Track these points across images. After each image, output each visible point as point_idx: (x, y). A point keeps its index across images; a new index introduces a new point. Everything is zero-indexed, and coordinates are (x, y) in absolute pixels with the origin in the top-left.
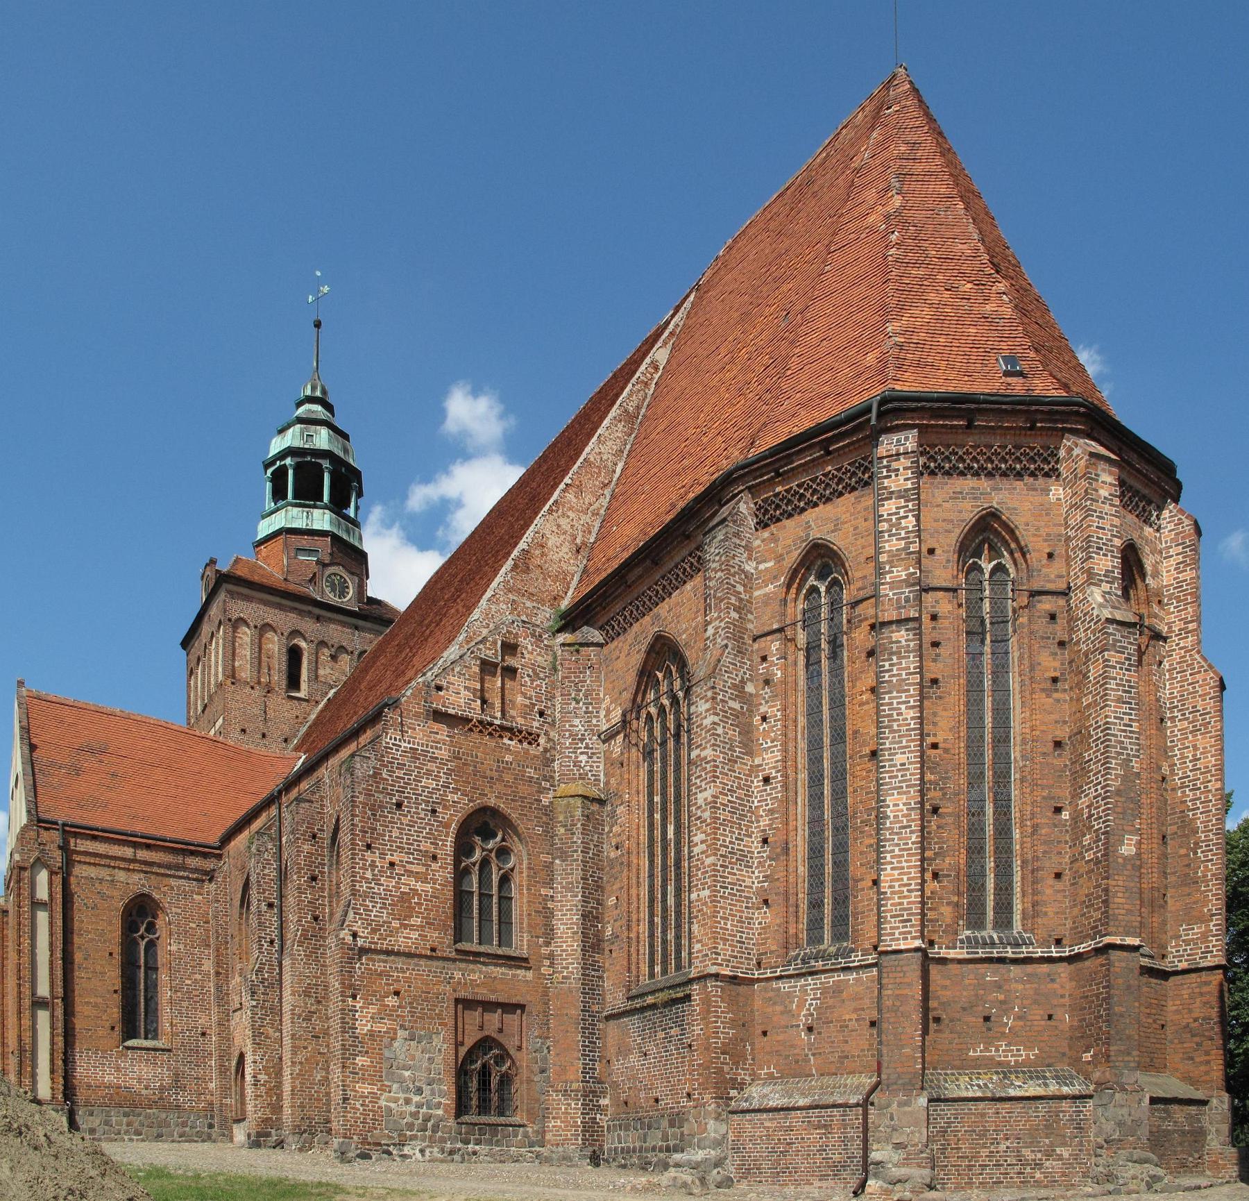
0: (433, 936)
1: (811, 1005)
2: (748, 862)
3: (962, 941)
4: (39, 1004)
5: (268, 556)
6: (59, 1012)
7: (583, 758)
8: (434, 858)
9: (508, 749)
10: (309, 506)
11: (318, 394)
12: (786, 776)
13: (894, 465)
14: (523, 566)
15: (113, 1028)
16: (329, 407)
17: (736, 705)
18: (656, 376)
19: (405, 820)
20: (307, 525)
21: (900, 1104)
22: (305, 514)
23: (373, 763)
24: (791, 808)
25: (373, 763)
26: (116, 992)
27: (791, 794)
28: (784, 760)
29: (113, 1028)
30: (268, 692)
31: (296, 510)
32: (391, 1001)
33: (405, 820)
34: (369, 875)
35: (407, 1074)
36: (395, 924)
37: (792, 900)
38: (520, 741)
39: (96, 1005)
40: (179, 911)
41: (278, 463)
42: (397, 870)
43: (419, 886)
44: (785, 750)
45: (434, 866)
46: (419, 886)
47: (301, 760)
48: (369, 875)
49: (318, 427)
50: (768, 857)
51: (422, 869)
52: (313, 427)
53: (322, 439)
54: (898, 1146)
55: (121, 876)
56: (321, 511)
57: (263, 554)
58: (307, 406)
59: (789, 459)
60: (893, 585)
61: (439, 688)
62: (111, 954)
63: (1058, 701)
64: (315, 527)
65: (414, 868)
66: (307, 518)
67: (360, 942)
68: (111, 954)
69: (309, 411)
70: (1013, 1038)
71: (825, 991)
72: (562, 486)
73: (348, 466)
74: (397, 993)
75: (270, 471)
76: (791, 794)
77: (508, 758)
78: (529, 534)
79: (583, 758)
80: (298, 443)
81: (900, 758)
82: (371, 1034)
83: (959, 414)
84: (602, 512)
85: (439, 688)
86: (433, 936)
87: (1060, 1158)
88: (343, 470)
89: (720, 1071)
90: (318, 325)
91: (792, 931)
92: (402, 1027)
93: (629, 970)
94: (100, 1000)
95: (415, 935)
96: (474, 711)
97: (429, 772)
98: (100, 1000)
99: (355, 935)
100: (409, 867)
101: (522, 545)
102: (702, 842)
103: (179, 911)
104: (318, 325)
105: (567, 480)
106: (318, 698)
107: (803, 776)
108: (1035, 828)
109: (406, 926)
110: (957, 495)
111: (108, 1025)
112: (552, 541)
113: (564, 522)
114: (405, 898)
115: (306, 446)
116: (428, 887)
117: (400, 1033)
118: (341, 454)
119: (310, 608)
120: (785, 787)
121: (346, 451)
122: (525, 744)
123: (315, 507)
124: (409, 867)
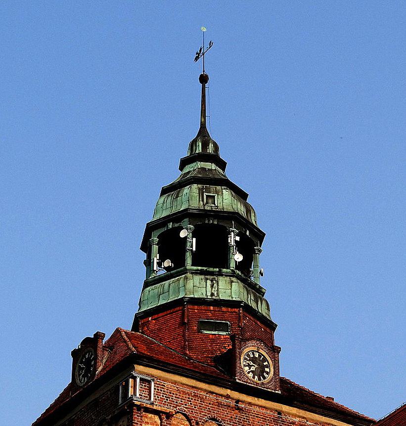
2: (158, 397)
5: (160, 330)
10: (212, 274)
11: (210, 149)
16: (222, 165)
20: (212, 294)
22: (209, 282)
31: (197, 278)
41: (170, 226)
49: (219, 188)
52: (213, 188)
56: (228, 279)
57: (151, 326)
64: (222, 297)
66: (212, 286)
69: (203, 169)
80: (196, 204)
88: (248, 233)
90: (204, 79)
104: (204, 79)
115: (207, 208)
119: (229, 392)
121: (249, 209)
123: (220, 274)
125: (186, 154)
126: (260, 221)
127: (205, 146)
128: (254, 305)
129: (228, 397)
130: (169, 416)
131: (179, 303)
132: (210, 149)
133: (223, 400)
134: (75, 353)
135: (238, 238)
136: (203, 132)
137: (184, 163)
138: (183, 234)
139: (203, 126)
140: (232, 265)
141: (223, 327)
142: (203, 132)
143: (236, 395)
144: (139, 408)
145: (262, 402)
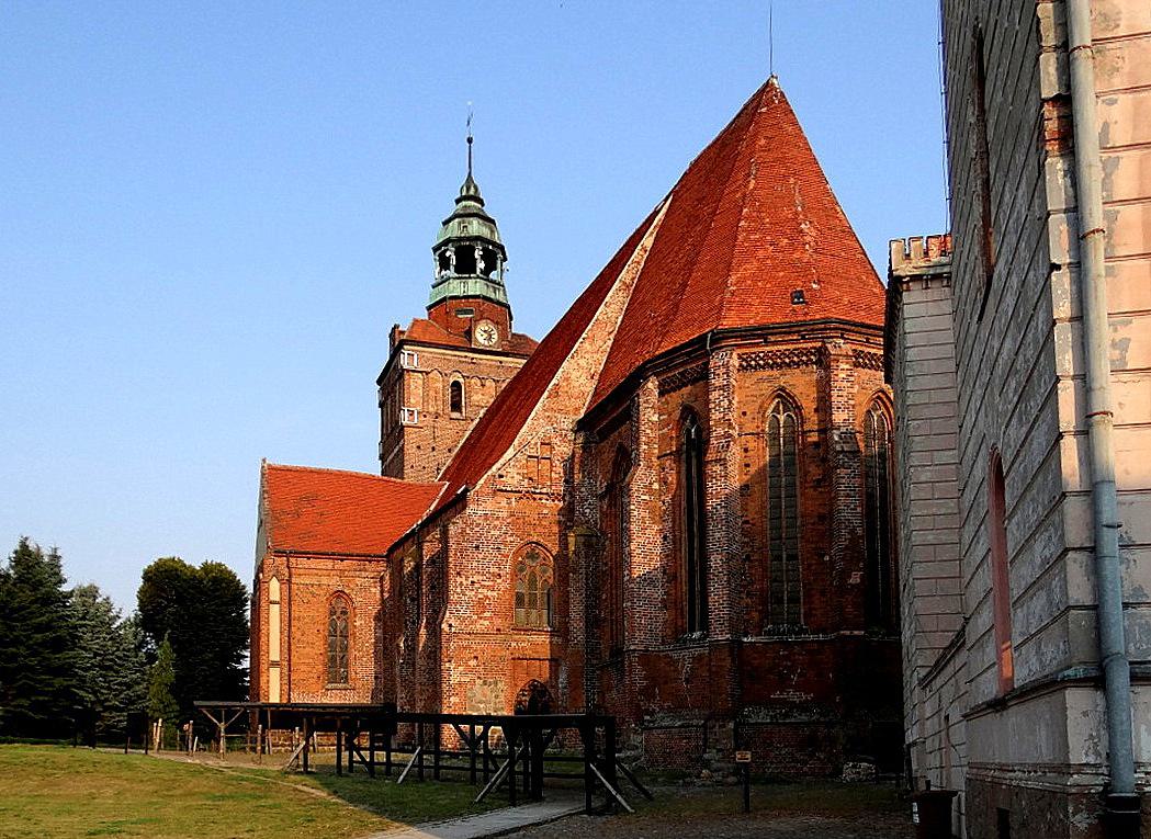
0: (498, 622)
3: (765, 632)
4: (275, 664)
6: (286, 670)
7: (588, 511)
9: (546, 507)
11: (472, 192)
12: (674, 536)
13: (717, 372)
14: (556, 393)
17: (647, 497)
18: (645, 256)
19: (481, 556)
21: (720, 726)
24: (678, 553)
27: (678, 545)
28: (673, 527)
32: (473, 663)
33: (481, 556)
34: (459, 590)
35: (482, 706)
36: (475, 617)
37: (679, 606)
38: (553, 501)
43: (489, 593)
44: (674, 521)
46: (489, 593)
47: (446, 487)
48: (459, 590)
51: (491, 583)
53: (476, 228)
54: (719, 751)
55: (325, 581)
59: (672, 360)
60: (717, 438)
61: (501, 476)
63: (821, 492)
65: (486, 583)
67: (453, 630)
70: (797, 688)
72: (581, 340)
73: (494, 244)
74: (476, 658)
75: (438, 253)
76: (678, 545)
77: (545, 511)
81: (717, 535)
82: (460, 684)
83: (759, 336)
84: (608, 350)
85: (501, 476)
86: (498, 622)
87: (819, 758)
88: (490, 247)
89: (638, 706)
90: (470, 141)
91: (680, 624)
92: (479, 678)
93: (612, 639)
95: (486, 623)
97: (495, 527)
99: (450, 626)
100: (483, 583)
101: (554, 381)
104: (470, 141)
105: (584, 335)
106: (473, 417)
107: (685, 535)
108: (810, 565)
109: (481, 618)
110: (761, 380)
111: (315, 676)
112: (574, 375)
113: (583, 362)
114: (480, 601)
116: (495, 594)
117: (477, 681)
119: (467, 354)
120: (674, 543)
122: (556, 502)
123: (470, 278)
124: (483, 583)
125: (459, 196)
126: (502, 237)
127: (468, 190)
128: (493, 296)
129: (466, 357)
130: (427, 373)
131: (444, 299)
132: (472, 192)
133: (464, 359)
134: (379, 382)
135: (481, 253)
136: (471, 194)
137: (458, 201)
138: (448, 254)
139: (470, 173)
140: (478, 271)
141: (471, 312)
142: (471, 194)
143: (471, 355)
144: (408, 371)
145: (489, 357)
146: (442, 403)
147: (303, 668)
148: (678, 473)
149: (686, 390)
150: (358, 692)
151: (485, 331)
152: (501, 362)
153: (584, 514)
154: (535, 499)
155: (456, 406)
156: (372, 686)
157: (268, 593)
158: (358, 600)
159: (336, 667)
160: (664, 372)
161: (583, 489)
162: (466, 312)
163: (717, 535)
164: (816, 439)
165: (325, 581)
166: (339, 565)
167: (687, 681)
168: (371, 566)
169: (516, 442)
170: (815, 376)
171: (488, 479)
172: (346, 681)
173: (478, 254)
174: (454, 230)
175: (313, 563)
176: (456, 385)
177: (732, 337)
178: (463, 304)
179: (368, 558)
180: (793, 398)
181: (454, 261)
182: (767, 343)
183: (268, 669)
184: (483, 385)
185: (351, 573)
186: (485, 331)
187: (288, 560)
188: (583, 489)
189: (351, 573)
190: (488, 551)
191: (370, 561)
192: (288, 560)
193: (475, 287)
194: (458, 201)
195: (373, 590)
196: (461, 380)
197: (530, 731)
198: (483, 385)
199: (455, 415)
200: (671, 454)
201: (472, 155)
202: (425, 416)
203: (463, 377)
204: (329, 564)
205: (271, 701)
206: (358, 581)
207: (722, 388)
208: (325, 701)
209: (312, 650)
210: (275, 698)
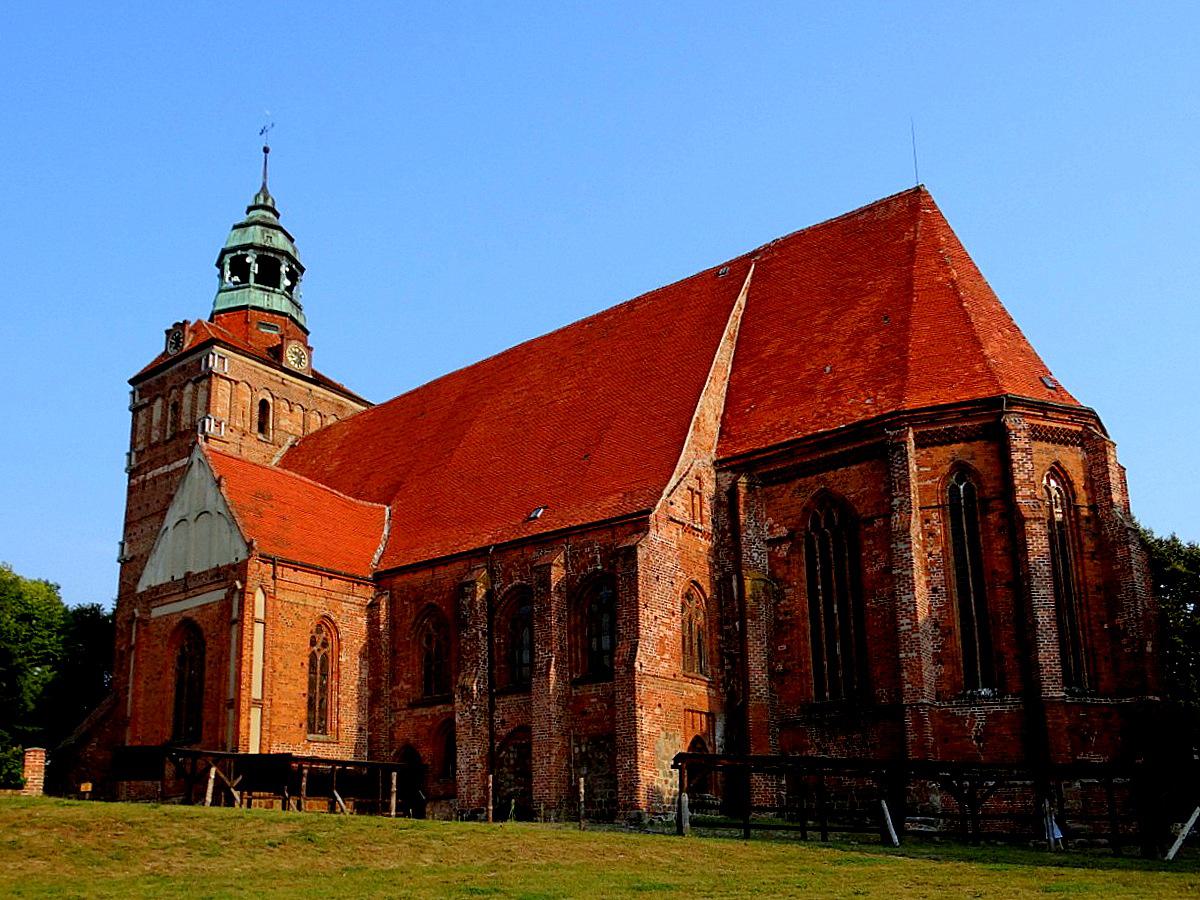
1: (978, 725)
4: (256, 703)
7: (755, 555)
8: (673, 614)
10: (269, 291)
15: (301, 725)
23: (647, 551)
25: (647, 551)
26: (304, 695)
29: (301, 725)
30: (244, 435)
32: (657, 711)
36: (658, 658)
39: (290, 707)
40: (347, 630)
42: (659, 621)
45: (674, 619)
50: (940, 635)
55: (310, 601)
58: (262, 212)
62: (302, 664)
68: (302, 664)
69: (265, 217)
71: (988, 717)
72: (709, 379)
78: (698, 410)
79: (755, 555)
81: (1042, 592)
90: (266, 150)
94: (292, 702)
96: (687, 520)
98: (292, 702)
99: (641, 666)
101: (696, 415)
102: (907, 624)
103: (347, 630)
104: (266, 150)
111: (297, 724)
118: (292, 254)
119: (278, 372)
123: (274, 292)
128: (295, 317)
129: (277, 375)
130: (237, 383)
131: (245, 307)
137: (250, 209)
139: (264, 185)
140: (282, 287)
144: (216, 375)
145: (299, 381)
146: (248, 420)
147: (284, 710)
148: (945, 526)
149: (957, 447)
150: (341, 745)
151: (295, 353)
152: (310, 390)
153: (751, 558)
154: (694, 534)
155: (262, 428)
156: (354, 740)
157: (253, 606)
158: (343, 630)
159: (317, 717)
160: (923, 425)
161: (750, 532)
162: (269, 327)
163: (1042, 592)
164: (1086, 514)
165: (310, 601)
166: (328, 583)
167: (978, 739)
168: (360, 590)
169: (677, 470)
170: (1080, 457)
171: (663, 505)
172: (325, 733)
173: (284, 269)
174: (237, 239)
175: (301, 577)
176: (264, 404)
177: (1021, 405)
178: (267, 318)
179: (355, 579)
180: (1065, 473)
181: (255, 269)
182: (1045, 417)
183: (249, 709)
184: (291, 411)
185: (339, 597)
186: (295, 353)
187: (274, 569)
188: (750, 532)
189: (339, 597)
190: (665, 582)
191: (359, 584)
192: (274, 569)
193: (279, 303)
194: (250, 209)
195: (359, 619)
196: (270, 400)
197: (886, 791)
198: (291, 411)
199: (260, 436)
200: (938, 506)
201: (263, 166)
202: (231, 431)
203: (272, 396)
204: (316, 580)
205: (250, 753)
206: (345, 607)
207: (1024, 450)
208: (305, 755)
209: (295, 688)
210: (254, 750)
